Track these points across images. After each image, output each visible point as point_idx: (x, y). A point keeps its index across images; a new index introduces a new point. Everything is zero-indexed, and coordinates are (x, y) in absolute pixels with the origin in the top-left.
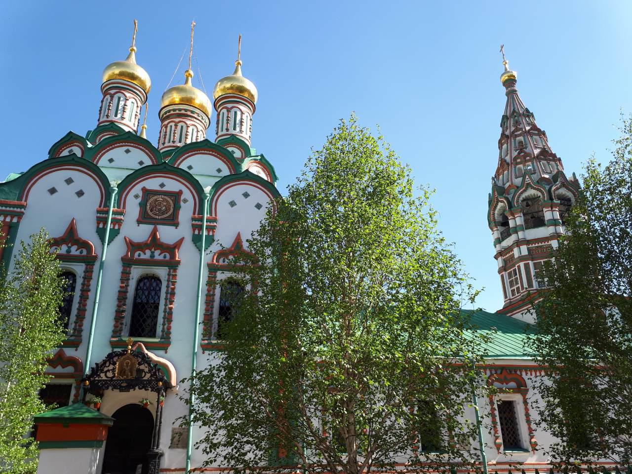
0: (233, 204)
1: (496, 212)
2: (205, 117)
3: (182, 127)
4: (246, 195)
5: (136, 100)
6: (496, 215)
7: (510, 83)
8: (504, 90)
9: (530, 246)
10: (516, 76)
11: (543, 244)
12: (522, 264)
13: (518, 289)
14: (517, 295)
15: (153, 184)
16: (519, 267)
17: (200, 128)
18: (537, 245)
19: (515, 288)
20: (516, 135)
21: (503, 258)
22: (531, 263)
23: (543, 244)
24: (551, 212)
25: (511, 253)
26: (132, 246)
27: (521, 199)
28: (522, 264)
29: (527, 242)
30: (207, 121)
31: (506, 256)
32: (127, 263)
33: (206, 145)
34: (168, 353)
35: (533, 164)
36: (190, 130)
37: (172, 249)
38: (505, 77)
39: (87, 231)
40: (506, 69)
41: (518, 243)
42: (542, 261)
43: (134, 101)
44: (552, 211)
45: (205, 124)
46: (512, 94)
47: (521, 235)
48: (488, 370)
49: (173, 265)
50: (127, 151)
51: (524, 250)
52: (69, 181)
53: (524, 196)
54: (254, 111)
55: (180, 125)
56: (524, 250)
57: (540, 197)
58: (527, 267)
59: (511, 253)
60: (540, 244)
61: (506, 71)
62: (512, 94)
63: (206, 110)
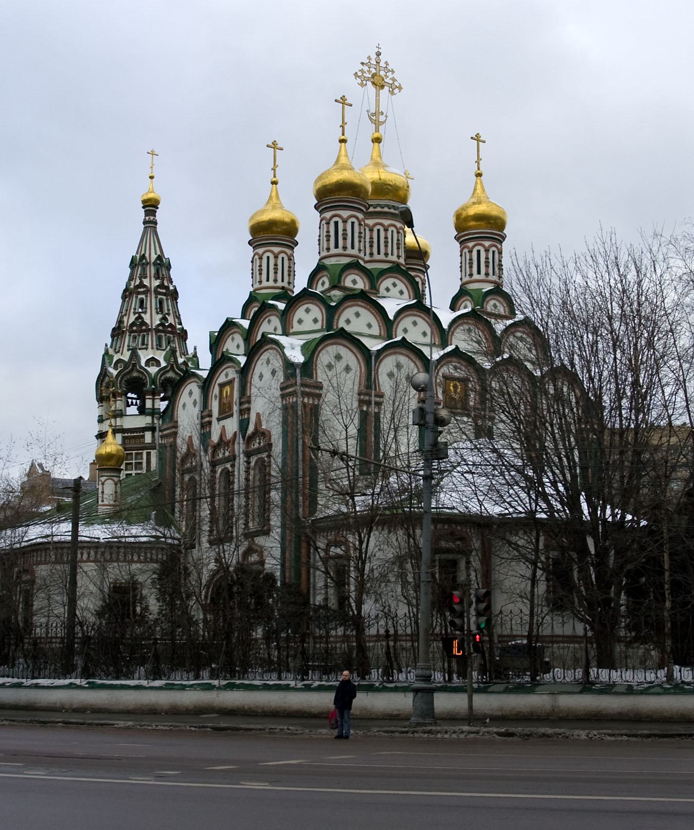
3: (268, 258)
7: (151, 206)
8: (141, 214)
9: (126, 435)
42: (134, 452)
46: (150, 224)
62: (150, 224)
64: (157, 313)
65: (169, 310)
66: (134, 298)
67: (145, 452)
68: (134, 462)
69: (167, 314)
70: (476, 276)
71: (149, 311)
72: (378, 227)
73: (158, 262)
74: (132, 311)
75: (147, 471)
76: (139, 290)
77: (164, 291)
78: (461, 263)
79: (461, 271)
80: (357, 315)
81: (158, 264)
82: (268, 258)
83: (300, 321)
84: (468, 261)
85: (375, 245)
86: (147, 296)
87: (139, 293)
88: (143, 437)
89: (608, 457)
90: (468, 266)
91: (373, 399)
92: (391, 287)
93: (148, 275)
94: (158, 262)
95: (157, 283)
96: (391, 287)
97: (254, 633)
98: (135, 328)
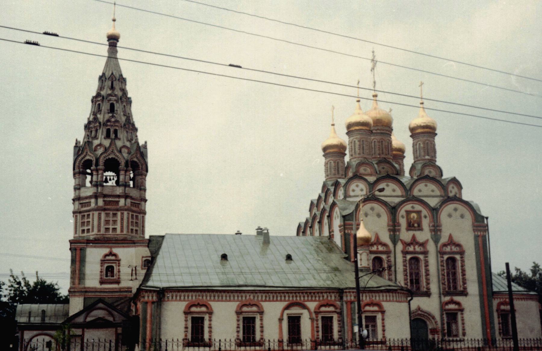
0: (450, 216)
15: (408, 207)
26: (406, 244)
32: (405, 253)
37: (423, 245)
39: (385, 238)
49: (425, 253)
50: (426, 186)
52: (456, 210)
80: (357, 186)
83: (353, 191)
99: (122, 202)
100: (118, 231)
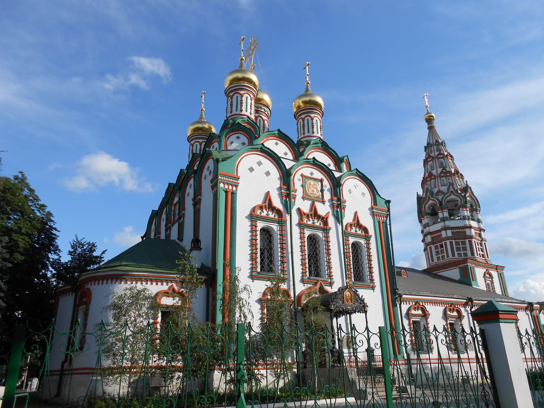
0: (251, 170)
1: (427, 206)
2: (266, 109)
3: (308, 120)
4: (260, 163)
5: (249, 95)
6: (426, 208)
7: (429, 120)
9: (453, 231)
10: (434, 116)
11: (461, 230)
12: (448, 242)
13: (443, 257)
14: (441, 260)
16: (445, 243)
17: (264, 118)
18: (457, 231)
19: (440, 256)
20: (439, 157)
21: (431, 236)
22: (453, 241)
23: (461, 230)
24: (442, 213)
25: (440, 233)
27: (447, 200)
28: (448, 242)
29: (452, 228)
30: (269, 113)
31: (434, 235)
33: (238, 126)
34: (487, 239)
35: (451, 178)
36: (315, 121)
38: (427, 116)
40: (428, 112)
41: (446, 229)
43: (247, 95)
44: (443, 212)
45: (268, 115)
46: (431, 128)
47: (448, 223)
48: (64, 372)
51: (449, 233)
53: (448, 198)
54: (323, 115)
55: (306, 119)
56: (449, 233)
57: (458, 200)
58: (451, 243)
59: (440, 233)
60: (459, 230)
61: (428, 113)
62: (431, 128)
63: (267, 104)
64: (440, 168)
65: (446, 165)
66: (426, 166)
67: (467, 241)
68: (439, 250)
69: (445, 167)
70: (306, 134)
71: (435, 168)
72: (196, 143)
73: (437, 143)
74: (438, 167)
75: (261, 270)
76: (429, 160)
77: (442, 156)
78: (298, 129)
79: (298, 133)
81: (438, 145)
82: (308, 120)
84: (302, 126)
85: (239, 102)
86: (433, 162)
87: (439, 158)
88: (441, 235)
89: (184, 399)
90: (302, 128)
91: (440, 256)
92: (255, 166)
93: (433, 151)
94: (437, 143)
95: (437, 153)
96: (255, 166)
97: (179, 392)
98: (442, 175)
99: (443, 234)
100: (450, 256)
